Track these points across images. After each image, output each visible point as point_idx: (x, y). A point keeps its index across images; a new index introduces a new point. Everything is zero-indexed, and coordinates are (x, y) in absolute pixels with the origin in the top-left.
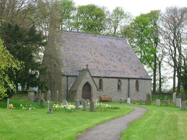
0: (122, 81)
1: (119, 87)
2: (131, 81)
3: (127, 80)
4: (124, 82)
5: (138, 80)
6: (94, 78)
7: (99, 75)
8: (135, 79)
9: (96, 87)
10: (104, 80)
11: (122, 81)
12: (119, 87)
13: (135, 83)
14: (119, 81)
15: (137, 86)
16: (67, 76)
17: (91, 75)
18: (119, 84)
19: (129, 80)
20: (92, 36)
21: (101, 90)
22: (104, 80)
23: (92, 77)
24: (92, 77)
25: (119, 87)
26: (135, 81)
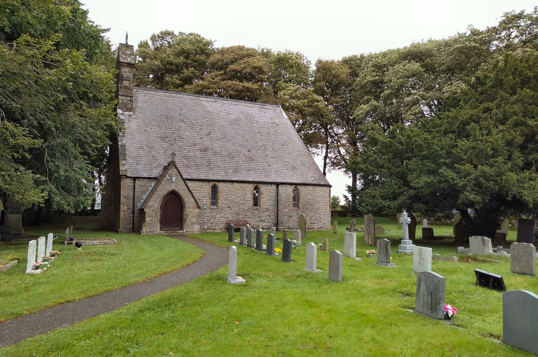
0: (263, 188)
1: (255, 202)
2: (281, 188)
3: (274, 187)
4: (268, 192)
5: (299, 187)
6: (187, 182)
7: (212, 178)
8: (291, 184)
9: (194, 201)
10: (221, 185)
11: (263, 188)
12: (256, 202)
13: (210, 190)
14: (256, 188)
15: (296, 198)
16: (135, 179)
17: (181, 176)
18: (257, 195)
19: (277, 188)
20: (208, 102)
21: (216, 207)
22: (221, 185)
23: (185, 180)
24: (185, 180)
25: (256, 202)
26: (290, 189)
